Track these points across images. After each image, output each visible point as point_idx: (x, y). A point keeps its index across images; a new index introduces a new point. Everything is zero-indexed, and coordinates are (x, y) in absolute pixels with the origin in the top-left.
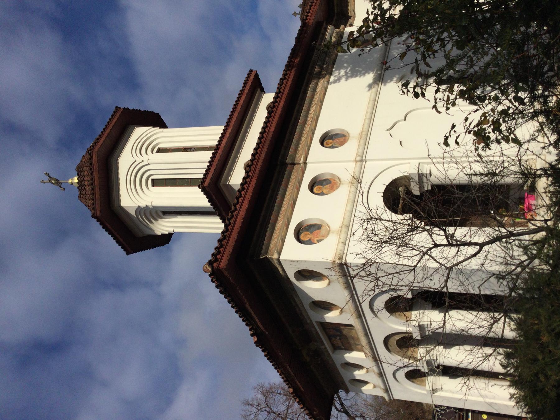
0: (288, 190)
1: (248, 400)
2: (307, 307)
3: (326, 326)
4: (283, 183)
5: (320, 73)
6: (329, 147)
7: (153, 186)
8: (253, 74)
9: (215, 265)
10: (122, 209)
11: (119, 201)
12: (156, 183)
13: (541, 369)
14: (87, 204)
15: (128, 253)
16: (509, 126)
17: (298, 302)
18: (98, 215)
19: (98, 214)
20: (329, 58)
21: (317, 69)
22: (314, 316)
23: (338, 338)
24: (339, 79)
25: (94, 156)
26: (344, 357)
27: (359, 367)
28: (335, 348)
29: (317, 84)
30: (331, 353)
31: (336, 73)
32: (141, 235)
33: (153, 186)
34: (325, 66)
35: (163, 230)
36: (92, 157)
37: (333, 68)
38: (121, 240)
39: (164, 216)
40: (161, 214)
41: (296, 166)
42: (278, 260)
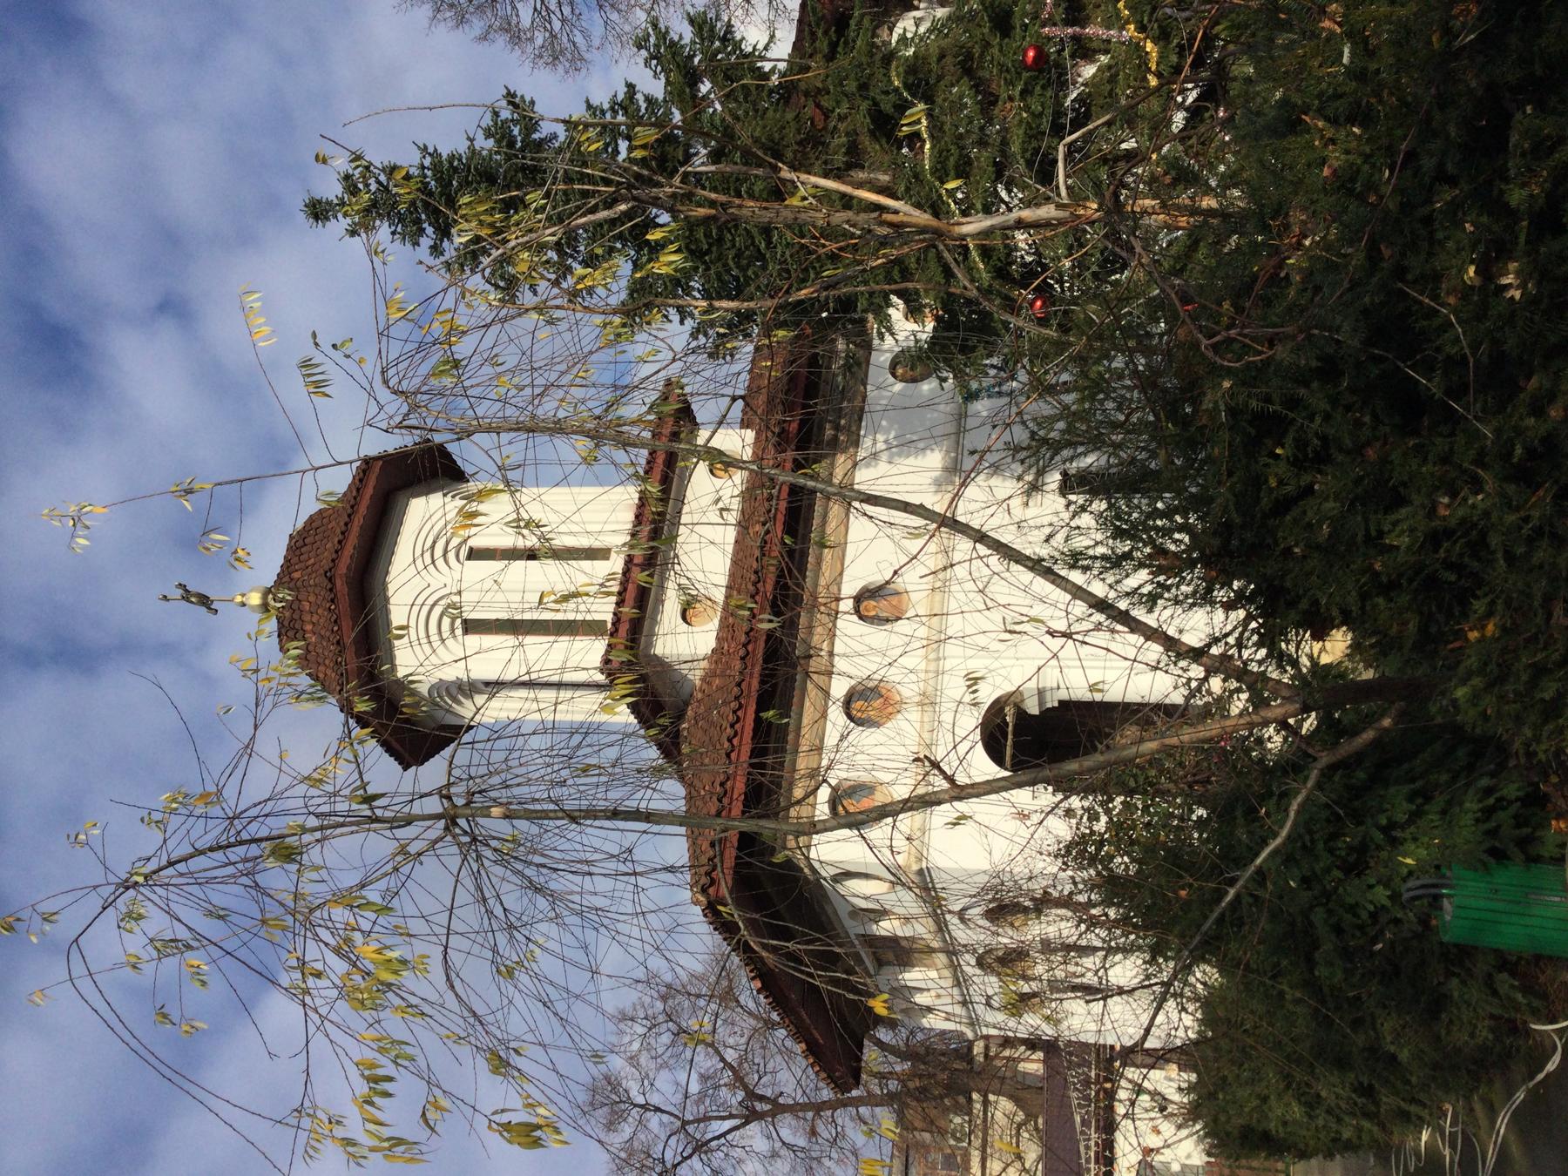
0: (805, 715)
3: (872, 941)
4: (795, 700)
5: (836, 438)
9: (711, 891)
13: (1481, 248)
17: (830, 911)
20: (849, 401)
21: (829, 432)
22: (854, 928)
24: (875, 456)
25: (339, 583)
27: (882, 913)
28: (880, 963)
31: (867, 443)
34: (843, 422)
36: (334, 584)
37: (859, 428)
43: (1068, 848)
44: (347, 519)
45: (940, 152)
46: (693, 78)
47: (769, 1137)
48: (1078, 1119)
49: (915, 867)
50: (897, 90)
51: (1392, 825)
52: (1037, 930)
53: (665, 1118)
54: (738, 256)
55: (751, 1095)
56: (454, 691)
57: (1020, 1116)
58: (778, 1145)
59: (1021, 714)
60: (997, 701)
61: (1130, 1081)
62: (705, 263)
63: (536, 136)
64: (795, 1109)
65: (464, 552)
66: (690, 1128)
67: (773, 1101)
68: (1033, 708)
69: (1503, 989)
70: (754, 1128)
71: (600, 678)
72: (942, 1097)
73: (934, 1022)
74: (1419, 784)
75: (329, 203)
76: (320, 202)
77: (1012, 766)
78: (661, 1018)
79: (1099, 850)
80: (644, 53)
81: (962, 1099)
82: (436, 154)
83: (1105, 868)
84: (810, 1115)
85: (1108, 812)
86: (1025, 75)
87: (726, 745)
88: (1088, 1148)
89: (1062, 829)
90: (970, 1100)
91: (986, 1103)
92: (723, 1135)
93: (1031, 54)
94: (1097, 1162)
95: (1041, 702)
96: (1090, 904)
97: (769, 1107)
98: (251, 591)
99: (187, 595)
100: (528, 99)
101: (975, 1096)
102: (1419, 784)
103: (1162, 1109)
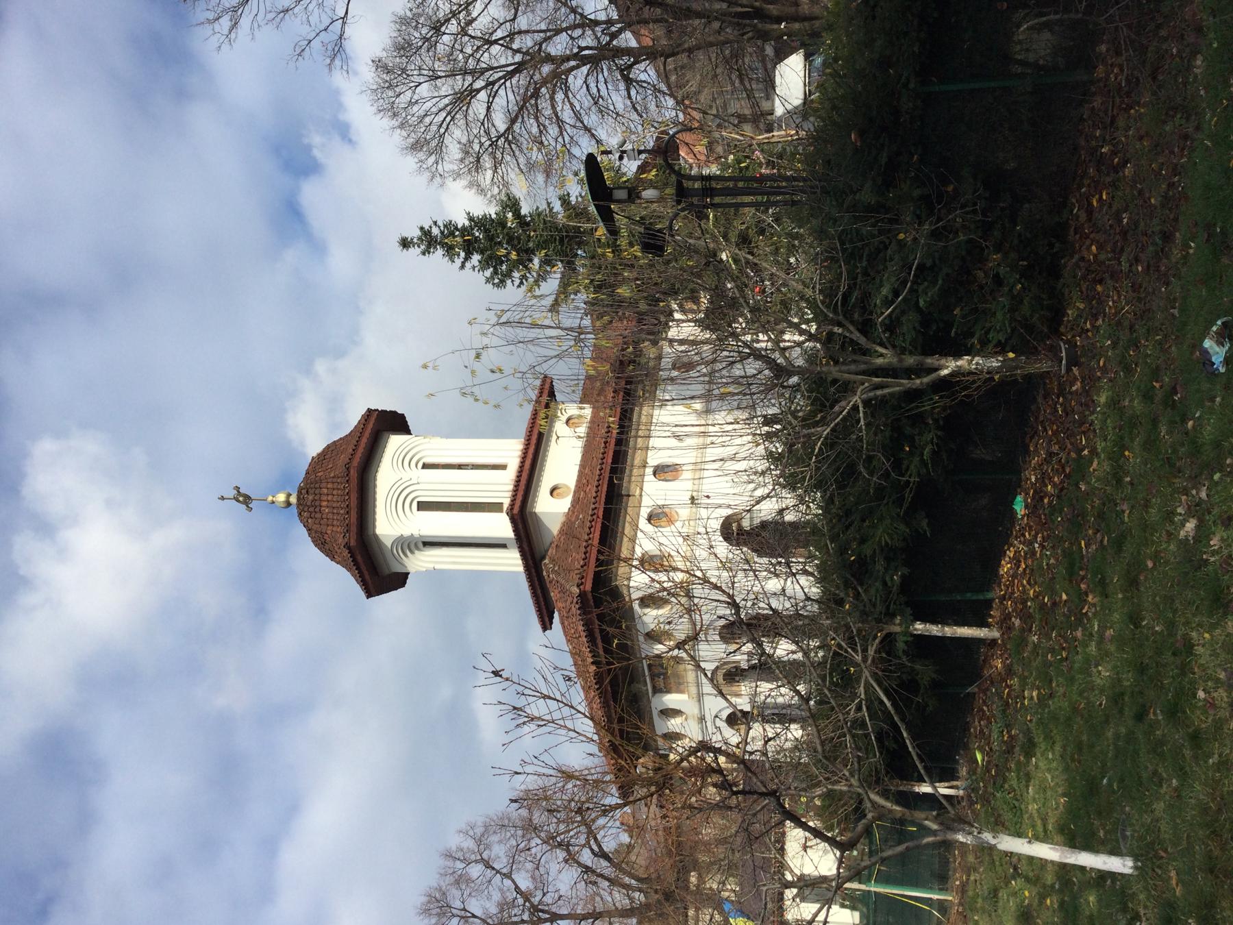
1: (450, 849)
6: (663, 480)
8: (548, 381)
9: (581, 587)
10: (376, 536)
11: (374, 527)
12: (423, 506)
15: (369, 595)
23: (662, 677)
25: (352, 471)
26: (663, 702)
28: (657, 690)
29: (641, 410)
30: (650, 695)
32: (387, 572)
35: (421, 567)
39: (425, 549)
40: (421, 545)
41: (631, 498)
65: (420, 465)
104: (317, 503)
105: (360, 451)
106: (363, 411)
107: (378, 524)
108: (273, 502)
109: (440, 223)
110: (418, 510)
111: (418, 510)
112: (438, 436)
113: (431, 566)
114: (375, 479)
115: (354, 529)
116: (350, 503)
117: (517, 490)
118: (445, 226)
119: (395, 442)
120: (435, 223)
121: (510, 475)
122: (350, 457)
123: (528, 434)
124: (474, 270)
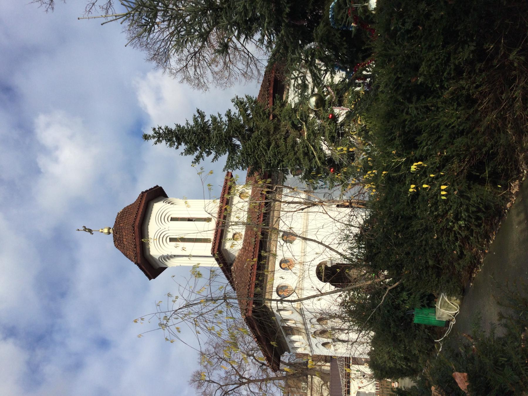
2: (279, 321)
7: (170, 241)
11: (149, 251)
14: (126, 253)
15: (150, 279)
16: (378, 57)
18: (139, 262)
19: (139, 262)
25: (136, 228)
28: (287, 334)
30: (285, 337)
33: (170, 241)
38: (148, 273)
42: (271, 306)
43: (341, 304)
44: (137, 210)
45: (309, 135)
46: (246, 110)
47: (247, 390)
48: (341, 375)
49: (299, 308)
50: (298, 119)
51: (404, 300)
52: (330, 323)
53: (215, 384)
54: (258, 155)
55: (241, 377)
56: (166, 258)
57: (322, 383)
58: (249, 393)
59: (326, 267)
60: (320, 264)
61: (332, 77)
62: (250, 157)
63: (205, 121)
64: (254, 381)
65: (169, 219)
66: (223, 388)
67: (248, 379)
68: (329, 265)
69: (426, 332)
70: (243, 387)
71: (212, 255)
72: (299, 377)
73: (299, 351)
74: (410, 292)
75: (150, 136)
76: (147, 135)
77: (324, 280)
78: (214, 354)
79: (347, 304)
80: (234, 103)
81: (305, 377)
82: (180, 126)
83: (349, 308)
84: (259, 383)
85: (349, 295)
86: (329, 120)
87: (249, 275)
88: (343, 383)
89: (340, 300)
90: (307, 377)
91: (312, 378)
92: (233, 389)
93: (331, 116)
94: (345, 387)
95: (331, 263)
96: (345, 317)
97: (247, 381)
98: (105, 228)
99: (85, 229)
100: (202, 111)
101: (309, 376)
102: (410, 292)
103: (364, 376)
104: (121, 239)
105: (141, 210)
106: (140, 193)
107: (151, 250)
108: (102, 232)
109: (163, 128)
110: (170, 241)
111: (170, 241)
112: (178, 198)
113: (179, 265)
114: (148, 229)
115: (139, 255)
116: (136, 243)
117: (221, 213)
118: (165, 129)
119: (158, 207)
120: (161, 128)
121: (212, 225)
122: (134, 220)
123: (214, 245)
124: (182, 155)
